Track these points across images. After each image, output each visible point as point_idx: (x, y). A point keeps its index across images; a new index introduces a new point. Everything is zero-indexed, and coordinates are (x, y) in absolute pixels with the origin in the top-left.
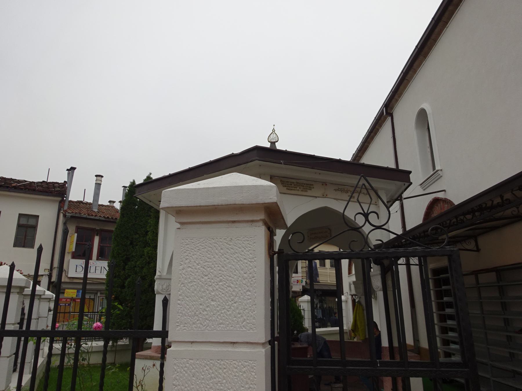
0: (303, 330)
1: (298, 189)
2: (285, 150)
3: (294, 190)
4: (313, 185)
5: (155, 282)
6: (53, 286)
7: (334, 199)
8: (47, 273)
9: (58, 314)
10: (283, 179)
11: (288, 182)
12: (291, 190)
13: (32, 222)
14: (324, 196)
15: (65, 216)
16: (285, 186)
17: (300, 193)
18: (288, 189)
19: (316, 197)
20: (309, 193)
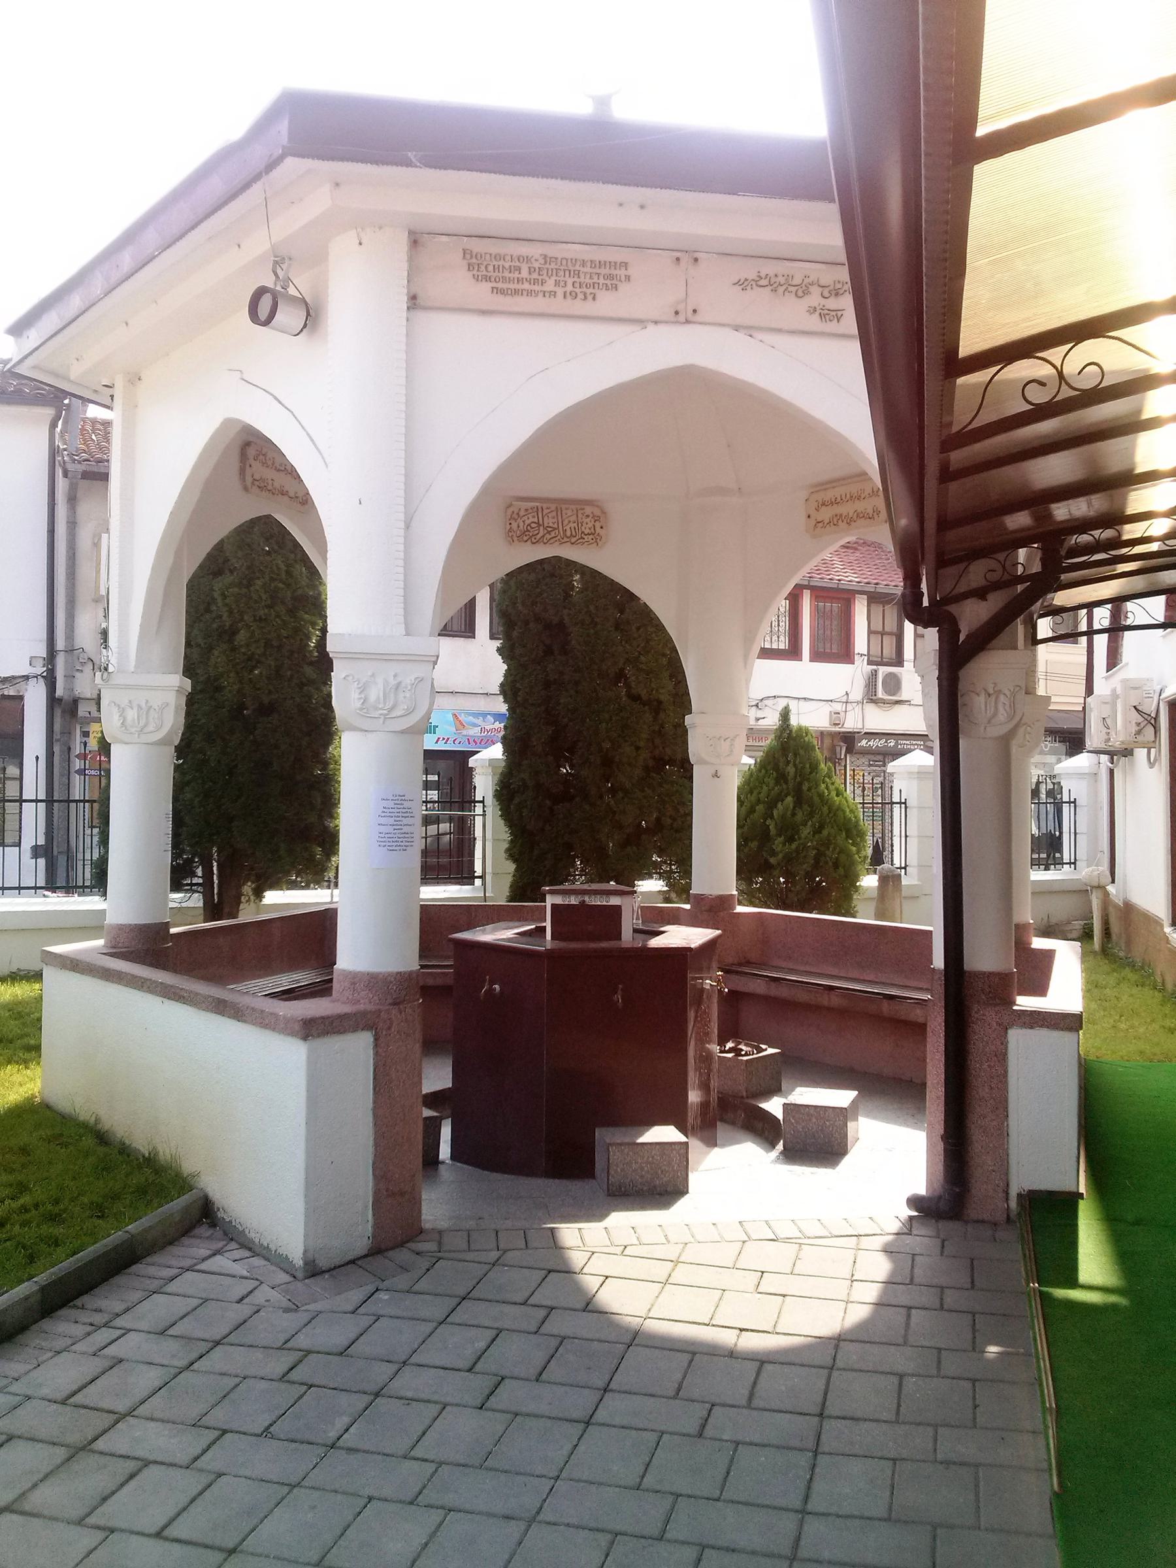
0: (185, 878)
1: (550, 285)
2: (579, 106)
3: (530, 293)
4: (625, 265)
5: (502, 685)
6: (63, 712)
7: (737, 328)
8: (40, 669)
9: (42, 796)
10: (478, 246)
11: (498, 257)
12: (516, 292)
13: (826, 514)
14: (684, 315)
15: (65, 474)
16: (487, 279)
17: (558, 304)
18: (502, 292)
19: (641, 322)
20: (606, 302)
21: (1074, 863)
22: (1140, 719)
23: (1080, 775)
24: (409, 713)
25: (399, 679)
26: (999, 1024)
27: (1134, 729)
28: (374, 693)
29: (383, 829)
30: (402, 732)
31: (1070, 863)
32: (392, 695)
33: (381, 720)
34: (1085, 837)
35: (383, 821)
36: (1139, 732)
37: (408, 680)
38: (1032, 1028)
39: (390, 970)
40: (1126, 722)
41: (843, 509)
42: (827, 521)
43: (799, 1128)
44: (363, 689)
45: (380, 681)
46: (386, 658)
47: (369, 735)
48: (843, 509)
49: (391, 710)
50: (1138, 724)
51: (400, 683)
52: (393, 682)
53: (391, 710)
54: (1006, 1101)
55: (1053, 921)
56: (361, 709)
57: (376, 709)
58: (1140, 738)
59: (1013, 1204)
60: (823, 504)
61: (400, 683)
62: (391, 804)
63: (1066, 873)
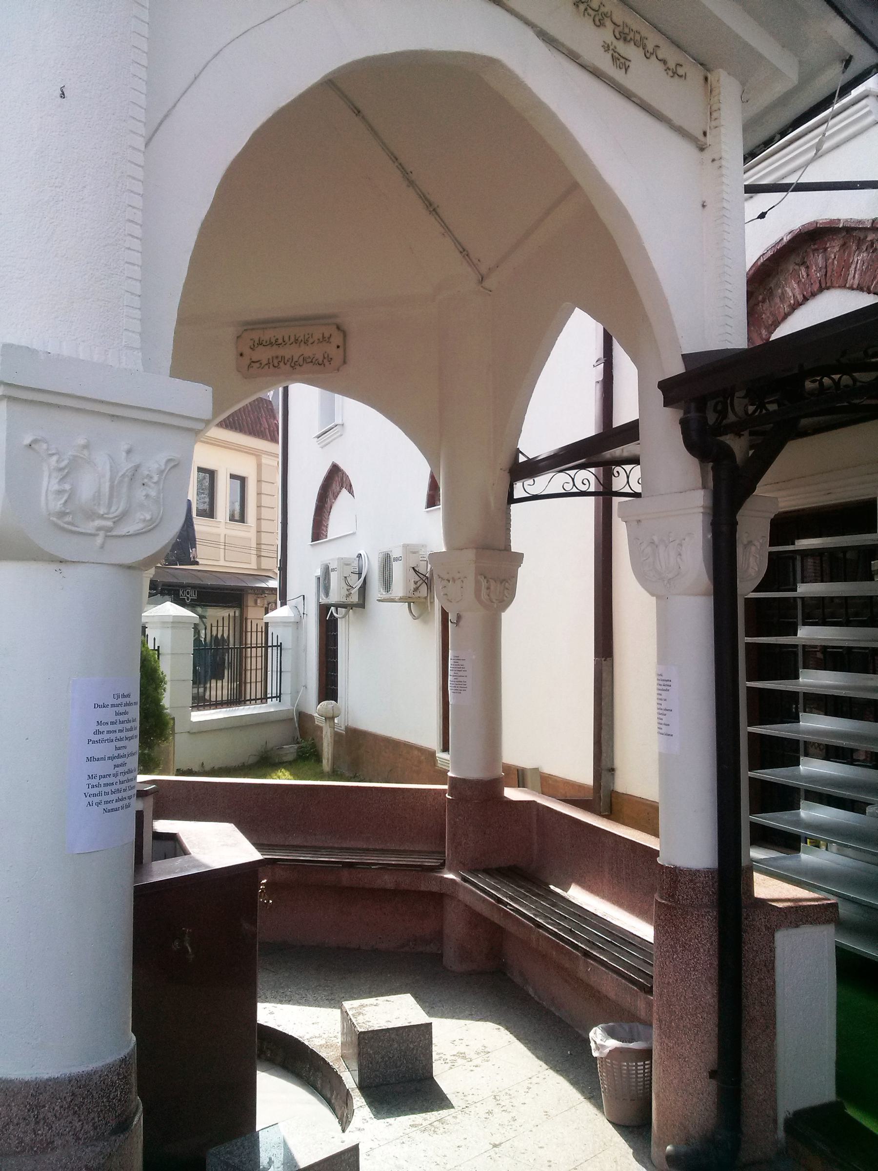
13: (264, 354)
21: (280, 697)
22: (417, 579)
23: (284, 623)
24: (152, 527)
25: (136, 459)
26: (767, 928)
27: (413, 586)
28: (87, 486)
29: (98, 768)
30: (121, 566)
31: (276, 697)
32: (124, 490)
33: (99, 540)
34: (289, 675)
35: (99, 750)
36: (416, 589)
37: (155, 463)
38: (797, 926)
39: (110, 1060)
40: (407, 581)
41: (286, 352)
42: (264, 362)
43: (378, 1058)
44: (67, 472)
45: (101, 460)
46: (116, 413)
47: (67, 570)
48: (286, 352)
49: (119, 519)
50: (416, 583)
51: (137, 468)
52: (125, 466)
53: (119, 519)
54: (775, 1016)
55: (270, 746)
56: (62, 514)
57: (91, 515)
58: (417, 594)
59: (781, 1134)
60: (260, 344)
61: (137, 468)
62: (108, 715)
63: (274, 705)
